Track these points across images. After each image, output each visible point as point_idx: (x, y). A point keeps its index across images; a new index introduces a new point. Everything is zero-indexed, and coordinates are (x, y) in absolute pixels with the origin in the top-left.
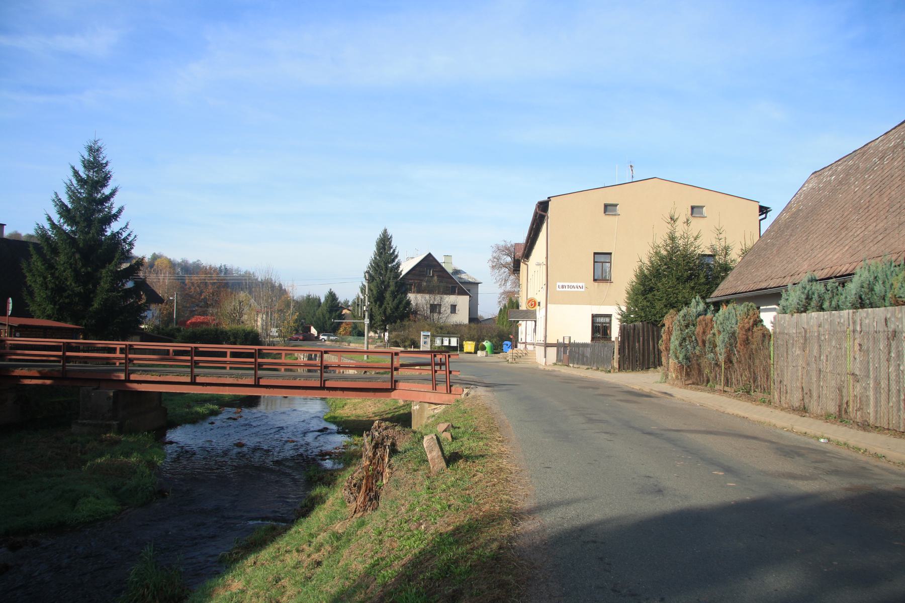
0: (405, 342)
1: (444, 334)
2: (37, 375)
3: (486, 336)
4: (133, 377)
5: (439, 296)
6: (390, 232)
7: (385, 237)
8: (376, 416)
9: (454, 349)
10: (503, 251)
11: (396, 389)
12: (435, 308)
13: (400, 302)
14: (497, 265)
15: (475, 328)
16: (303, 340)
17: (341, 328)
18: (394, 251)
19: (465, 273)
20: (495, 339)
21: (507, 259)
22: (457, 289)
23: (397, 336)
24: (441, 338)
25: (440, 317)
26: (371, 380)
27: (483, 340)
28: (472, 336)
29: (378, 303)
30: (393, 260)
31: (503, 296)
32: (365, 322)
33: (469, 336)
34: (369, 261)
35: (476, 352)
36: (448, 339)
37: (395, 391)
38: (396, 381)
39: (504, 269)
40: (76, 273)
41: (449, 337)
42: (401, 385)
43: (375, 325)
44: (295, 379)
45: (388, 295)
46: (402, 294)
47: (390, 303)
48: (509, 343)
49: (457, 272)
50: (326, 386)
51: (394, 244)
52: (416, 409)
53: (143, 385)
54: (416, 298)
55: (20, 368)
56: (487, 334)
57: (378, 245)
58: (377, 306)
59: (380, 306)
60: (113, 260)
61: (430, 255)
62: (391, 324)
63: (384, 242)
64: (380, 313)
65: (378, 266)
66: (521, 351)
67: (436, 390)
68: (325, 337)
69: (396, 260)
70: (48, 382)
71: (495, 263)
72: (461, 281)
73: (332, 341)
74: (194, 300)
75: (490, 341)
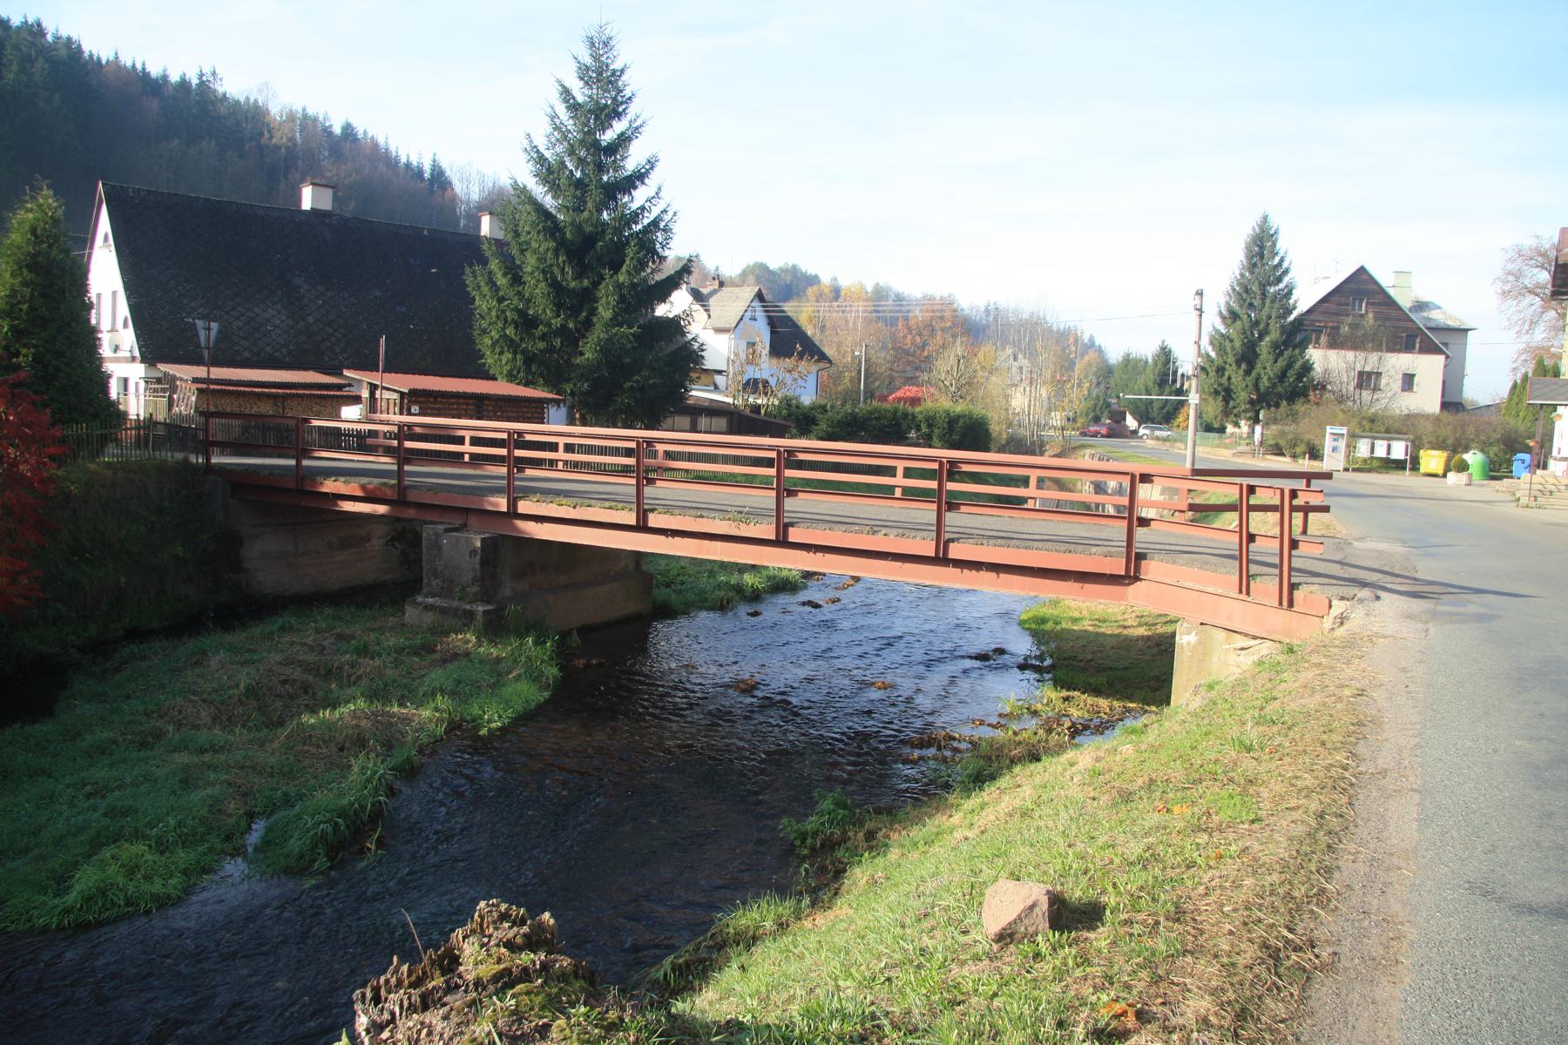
0: (1295, 446)
1: (1377, 432)
2: (360, 493)
3: (1473, 440)
4: (524, 507)
5: (1375, 354)
6: (1274, 222)
7: (1264, 232)
8: (1140, 625)
9: (1399, 465)
10: (1532, 259)
11: (1141, 580)
12: (1367, 380)
13: (1290, 366)
14: (1514, 288)
15: (1449, 424)
16: (1108, 436)
17: (1181, 416)
18: (1282, 260)
19: (1439, 308)
20: (1495, 449)
21: (1539, 276)
22: (1418, 340)
23: (1283, 434)
24: (1369, 441)
25: (1375, 397)
26: (1072, 547)
27: (1467, 449)
28: (1441, 439)
29: (1244, 366)
30: (1279, 280)
31: (1523, 357)
32: (1190, 401)
33: (1433, 439)
34: (1229, 283)
35: (1444, 476)
36: (1385, 443)
37: (1138, 583)
38: (1141, 557)
39: (1530, 298)
40: (556, 286)
41: (1389, 439)
42: (1151, 568)
43: (1235, 411)
44: (874, 533)
45: (1264, 347)
46: (1294, 348)
47: (1267, 368)
48: (1526, 457)
49: (1420, 306)
50: (951, 556)
51: (1281, 246)
52: (1189, 643)
53: (547, 526)
54: (1326, 358)
55: (333, 479)
56: (1477, 436)
57: (1248, 249)
58: (1241, 372)
59: (1248, 373)
60: (624, 262)
61: (1362, 270)
62: (1269, 408)
63: (1261, 239)
64: (1247, 386)
65: (1247, 291)
66: (1555, 477)
67: (1248, 593)
68: (1147, 432)
69: (1286, 280)
70: (381, 509)
71: (1510, 285)
72: (1429, 325)
73: (1158, 439)
74: (910, 358)
75: (1482, 451)
